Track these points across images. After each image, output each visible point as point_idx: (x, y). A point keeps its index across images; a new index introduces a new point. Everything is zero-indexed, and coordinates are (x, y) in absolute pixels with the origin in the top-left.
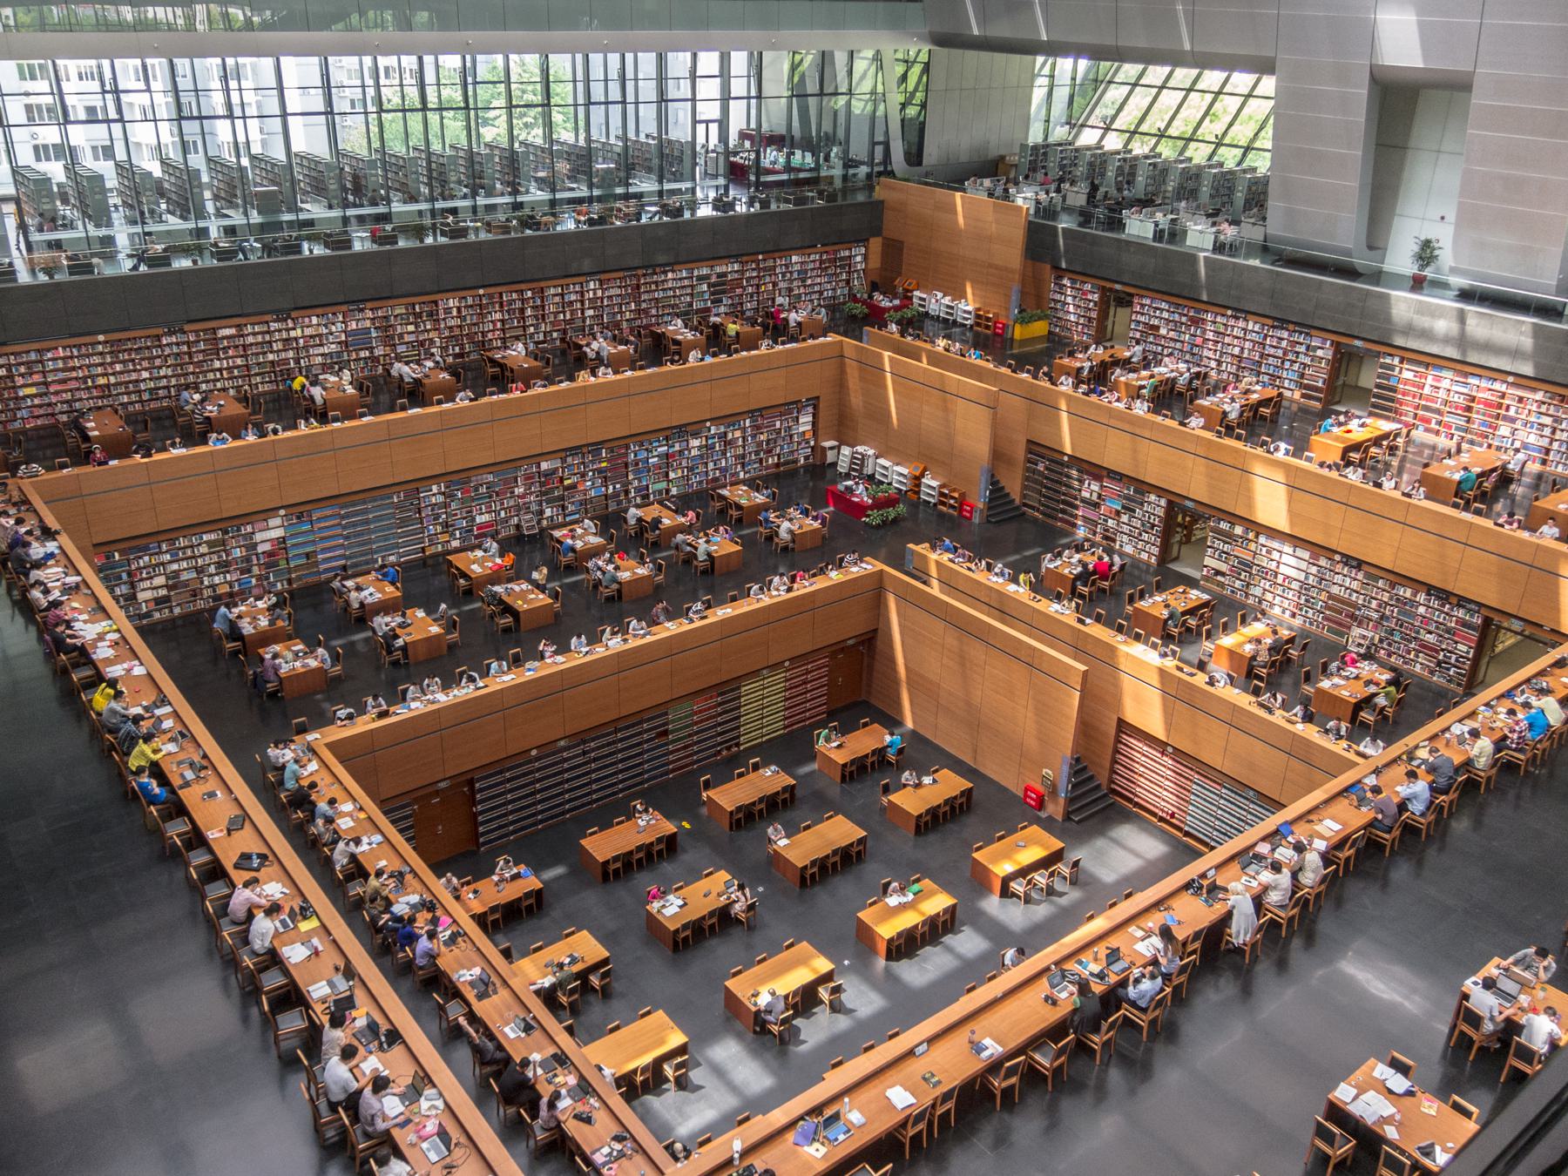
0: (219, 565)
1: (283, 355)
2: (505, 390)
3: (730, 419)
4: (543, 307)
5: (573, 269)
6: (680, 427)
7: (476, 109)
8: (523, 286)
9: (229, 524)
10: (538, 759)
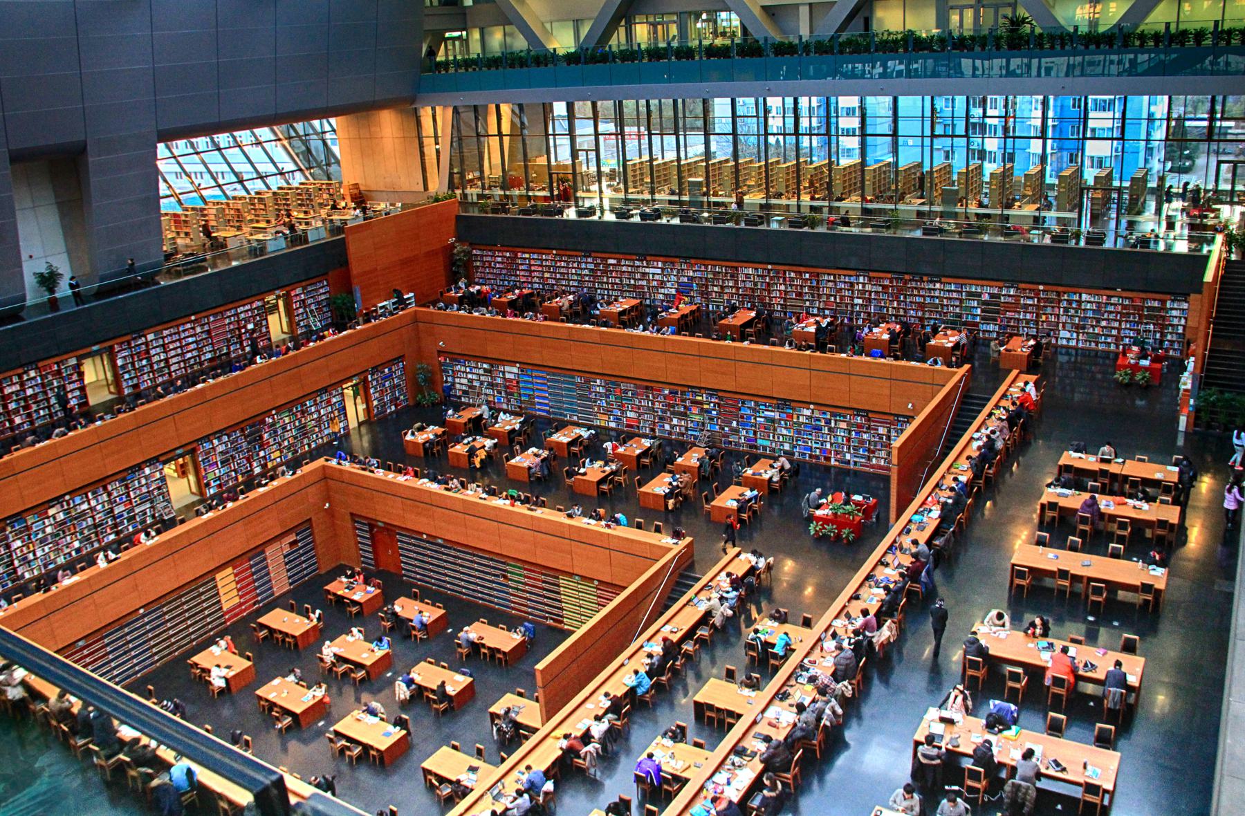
0: (489, 384)
1: (641, 283)
2: (692, 335)
7: (554, 135)
8: (802, 269)
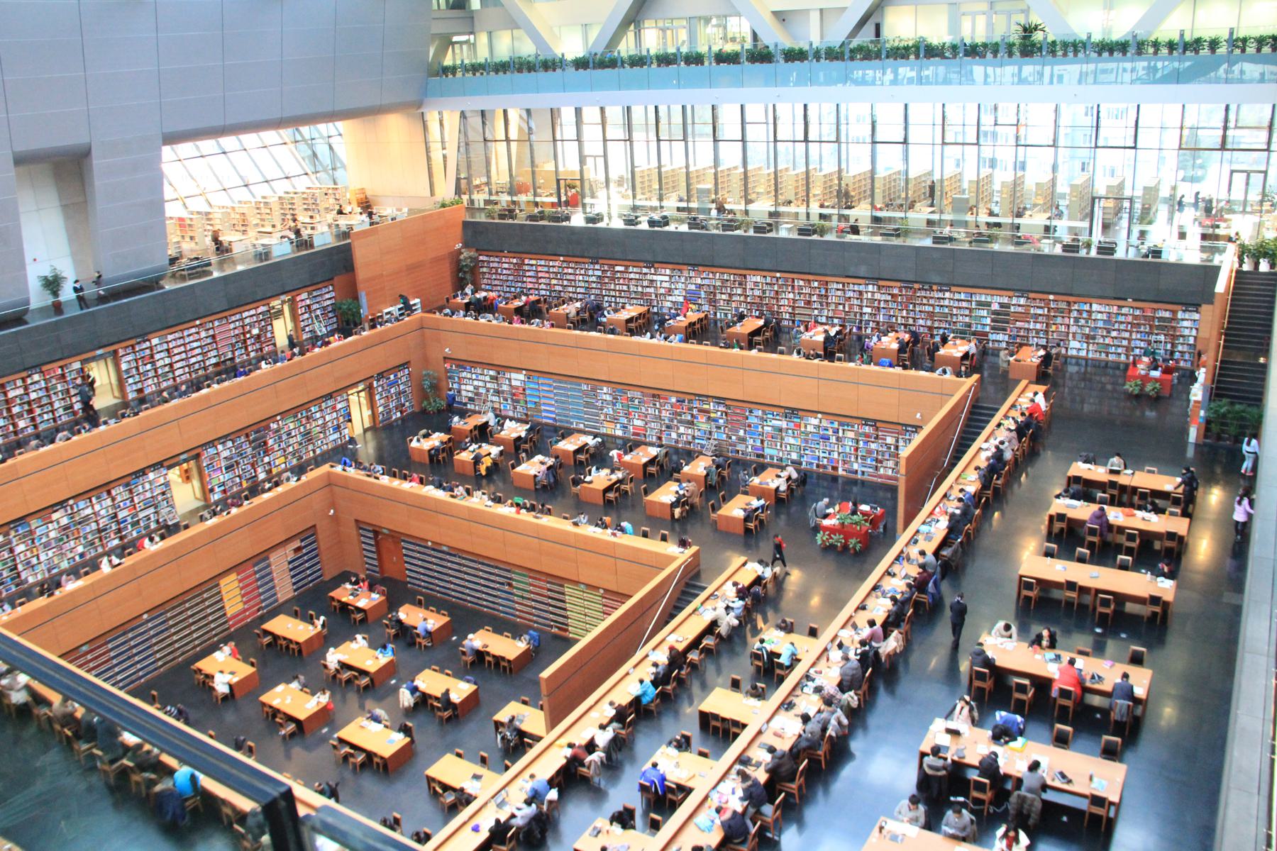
1: (648, 290)
3: (845, 420)
4: (827, 297)
5: (852, 271)
6: (793, 410)
8: (811, 277)
9: (502, 368)
10: (148, 621)
